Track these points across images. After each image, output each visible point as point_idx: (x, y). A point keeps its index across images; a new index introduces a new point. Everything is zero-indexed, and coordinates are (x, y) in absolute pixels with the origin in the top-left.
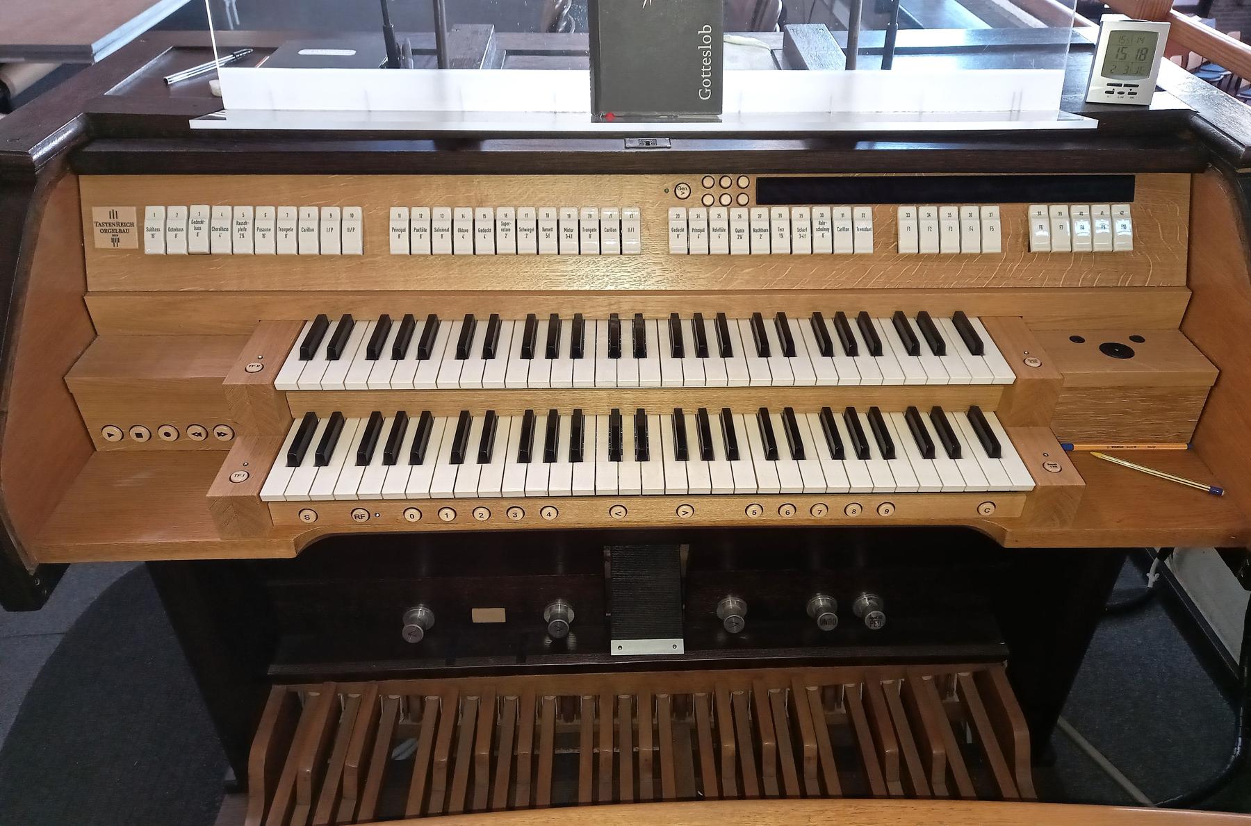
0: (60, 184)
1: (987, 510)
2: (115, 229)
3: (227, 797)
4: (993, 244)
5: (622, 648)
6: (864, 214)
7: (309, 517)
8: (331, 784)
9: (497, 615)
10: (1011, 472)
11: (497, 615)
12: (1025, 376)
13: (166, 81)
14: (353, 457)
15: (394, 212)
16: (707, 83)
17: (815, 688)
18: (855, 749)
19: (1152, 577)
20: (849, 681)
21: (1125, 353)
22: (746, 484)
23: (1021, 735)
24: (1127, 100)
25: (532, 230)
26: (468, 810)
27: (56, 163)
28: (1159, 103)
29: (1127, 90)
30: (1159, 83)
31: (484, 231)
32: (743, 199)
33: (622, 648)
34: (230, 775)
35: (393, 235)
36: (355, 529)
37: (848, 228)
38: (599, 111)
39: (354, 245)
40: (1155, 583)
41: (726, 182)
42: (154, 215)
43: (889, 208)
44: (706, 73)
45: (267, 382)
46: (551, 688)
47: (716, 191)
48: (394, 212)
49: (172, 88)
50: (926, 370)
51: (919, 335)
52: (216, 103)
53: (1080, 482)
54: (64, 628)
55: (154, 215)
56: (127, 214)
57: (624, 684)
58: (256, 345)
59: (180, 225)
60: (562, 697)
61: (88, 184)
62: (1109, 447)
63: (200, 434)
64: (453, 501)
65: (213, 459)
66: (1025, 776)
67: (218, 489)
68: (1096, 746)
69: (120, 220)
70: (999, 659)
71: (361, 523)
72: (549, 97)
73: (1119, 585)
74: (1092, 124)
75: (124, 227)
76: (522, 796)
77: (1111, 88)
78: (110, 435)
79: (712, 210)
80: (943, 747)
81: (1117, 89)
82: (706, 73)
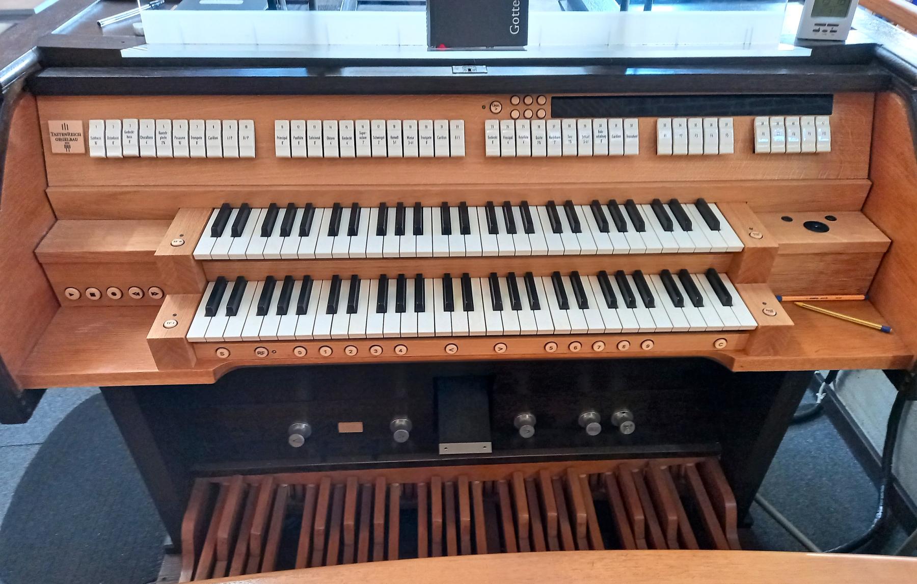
0: (22, 102)
1: (721, 345)
2: (67, 138)
3: (166, 557)
4: (728, 147)
5: (446, 449)
6: (632, 125)
7: (223, 354)
8: (241, 548)
9: (357, 427)
10: (740, 315)
11: (357, 427)
12: (751, 244)
13: (99, 24)
14: (255, 309)
15: (278, 124)
16: (516, 21)
17: (584, 476)
18: (415, 511)
19: (820, 396)
20: (605, 467)
21: (823, 228)
22: (545, 326)
23: (731, 505)
24: (829, 36)
25: (382, 138)
26: (340, 562)
27: (17, 88)
28: (853, 39)
29: (829, 29)
30: (853, 25)
31: (347, 138)
32: (541, 113)
33: (446, 449)
34: (168, 541)
35: (278, 142)
36: (257, 363)
37: (620, 135)
38: (435, 41)
39: (248, 151)
40: (822, 400)
41: (528, 100)
42: (96, 128)
43: (649, 120)
44: (516, 13)
45: (188, 253)
46: (398, 478)
47: (522, 107)
48: (278, 124)
49: (104, 30)
50: (677, 241)
51: (671, 213)
52: (140, 38)
53: (790, 322)
54: (42, 439)
55: (96, 128)
56: (75, 126)
57: (450, 472)
58: (178, 226)
59: (111, 134)
60: (404, 484)
61: (45, 106)
62: (808, 298)
63: (138, 294)
64: (330, 341)
65: (150, 310)
66: (733, 535)
67: (156, 332)
68: (781, 512)
69: (70, 131)
70: (715, 454)
71: (262, 357)
72: (404, 35)
73: (804, 402)
74: (807, 52)
75: (73, 137)
76: (378, 550)
77: (817, 28)
78: (71, 295)
79: (517, 121)
80: (675, 516)
81: (822, 28)
82: (516, 13)
